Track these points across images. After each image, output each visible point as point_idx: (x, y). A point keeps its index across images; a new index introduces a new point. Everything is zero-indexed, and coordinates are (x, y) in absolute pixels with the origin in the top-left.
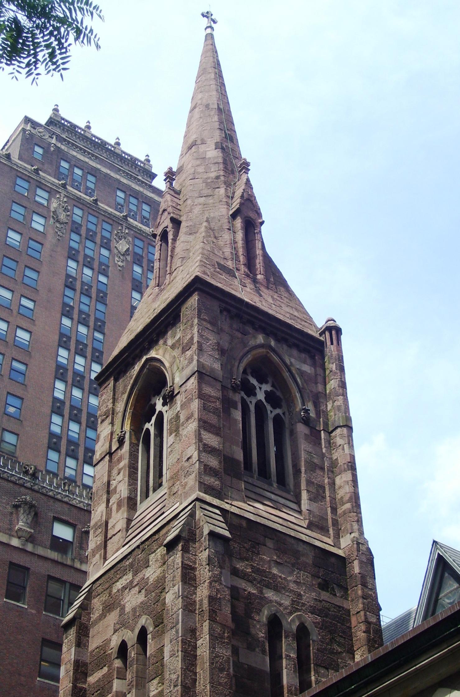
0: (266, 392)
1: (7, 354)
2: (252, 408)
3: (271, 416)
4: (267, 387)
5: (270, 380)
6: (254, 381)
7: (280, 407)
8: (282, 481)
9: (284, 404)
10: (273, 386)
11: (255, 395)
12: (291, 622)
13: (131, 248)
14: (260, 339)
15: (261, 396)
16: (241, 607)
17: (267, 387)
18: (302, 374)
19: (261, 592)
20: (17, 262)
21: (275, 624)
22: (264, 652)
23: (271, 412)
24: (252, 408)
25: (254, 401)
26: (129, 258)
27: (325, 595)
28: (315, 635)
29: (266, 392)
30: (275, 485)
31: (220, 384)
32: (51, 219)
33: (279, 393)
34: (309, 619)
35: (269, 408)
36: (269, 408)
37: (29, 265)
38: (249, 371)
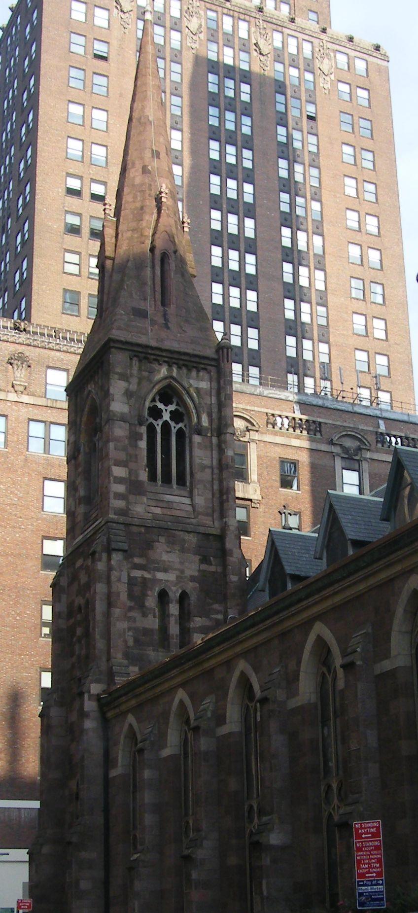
0: (171, 412)
1: (85, 176)
2: (159, 429)
3: (174, 431)
4: (172, 407)
5: (175, 400)
6: (160, 406)
7: (182, 421)
8: (181, 481)
9: (185, 418)
10: (177, 405)
11: (161, 417)
12: (174, 593)
13: (203, 24)
14: (164, 371)
15: (166, 416)
16: (137, 590)
17: (172, 407)
18: (198, 390)
19: (154, 576)
20: (84, 70)
21: (163, 596)
22: (155, 617)
23: (174, 427)
24: (159, 429)
25: (160, 422)
26: (202, 36)
27: (204, 567)
28: (193, 598)
29: (171, 412)
30: (175, 486)
31: (128, 425)
32: (115, 10)
33: (181, 409)
34: (190, 587)
35: (172, 424)
36: (172, 424)
37: (97, 71)
38: (157, 398)
